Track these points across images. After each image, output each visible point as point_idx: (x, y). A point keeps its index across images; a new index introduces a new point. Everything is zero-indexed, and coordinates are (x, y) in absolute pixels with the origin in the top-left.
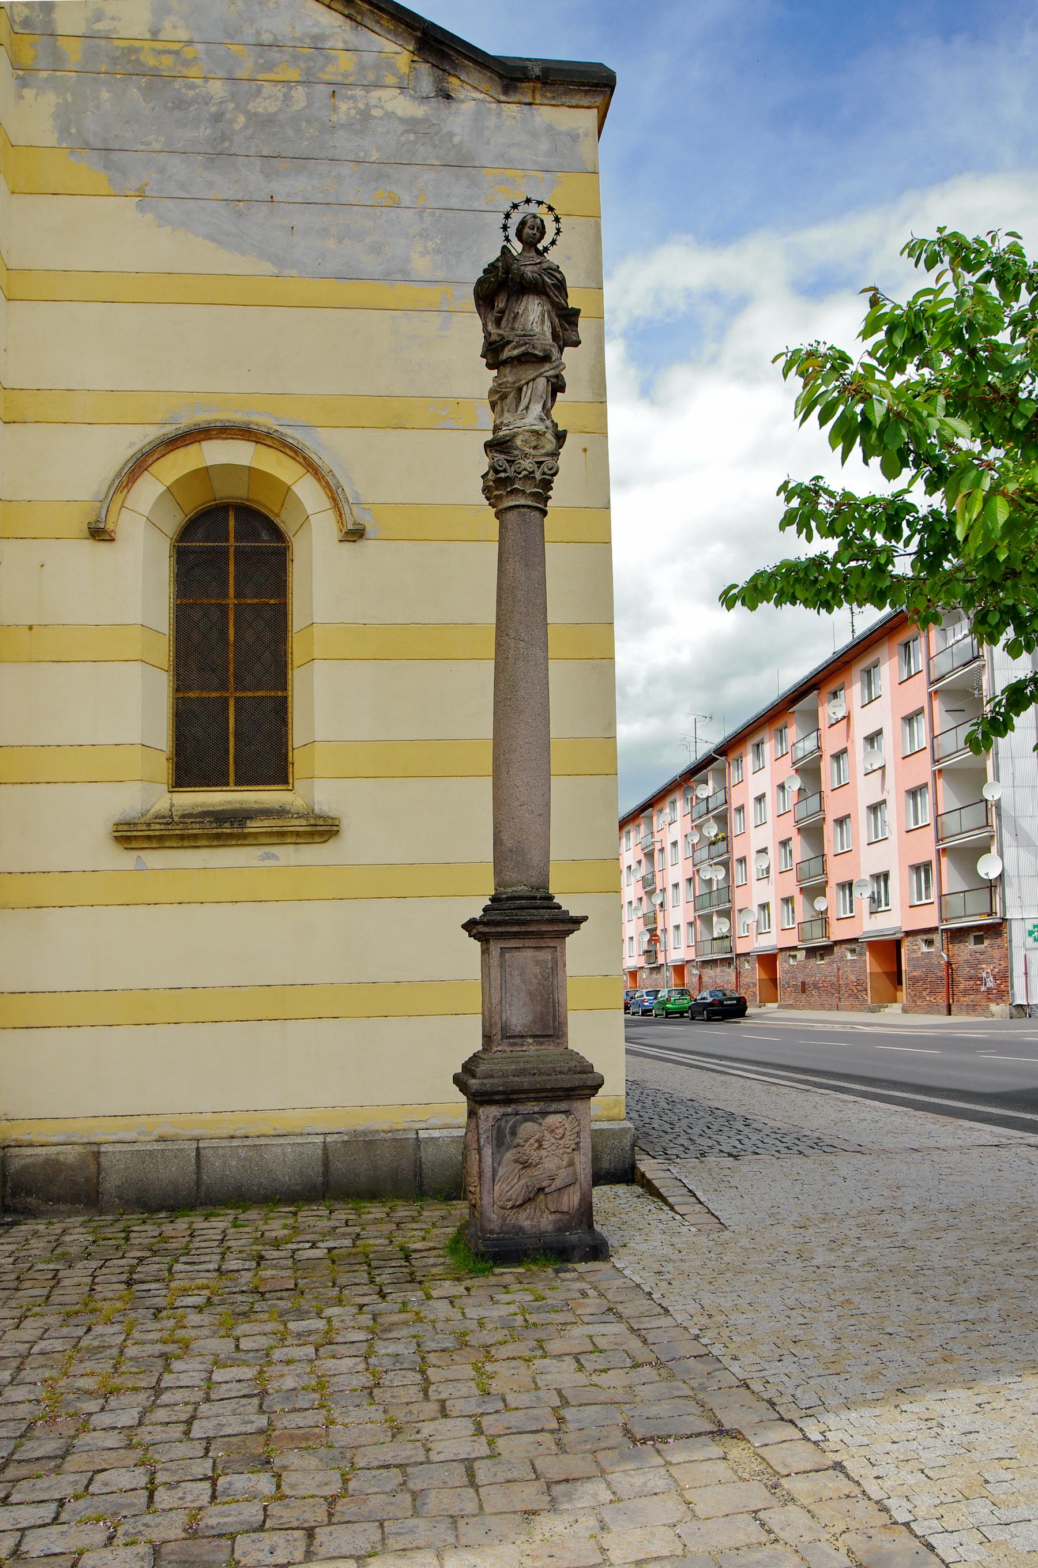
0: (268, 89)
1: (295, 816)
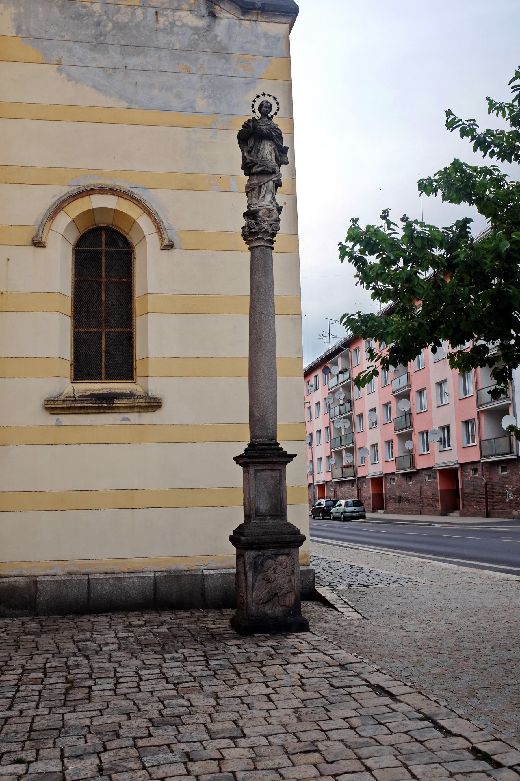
0: (123, 9)
1: (139, 397)
